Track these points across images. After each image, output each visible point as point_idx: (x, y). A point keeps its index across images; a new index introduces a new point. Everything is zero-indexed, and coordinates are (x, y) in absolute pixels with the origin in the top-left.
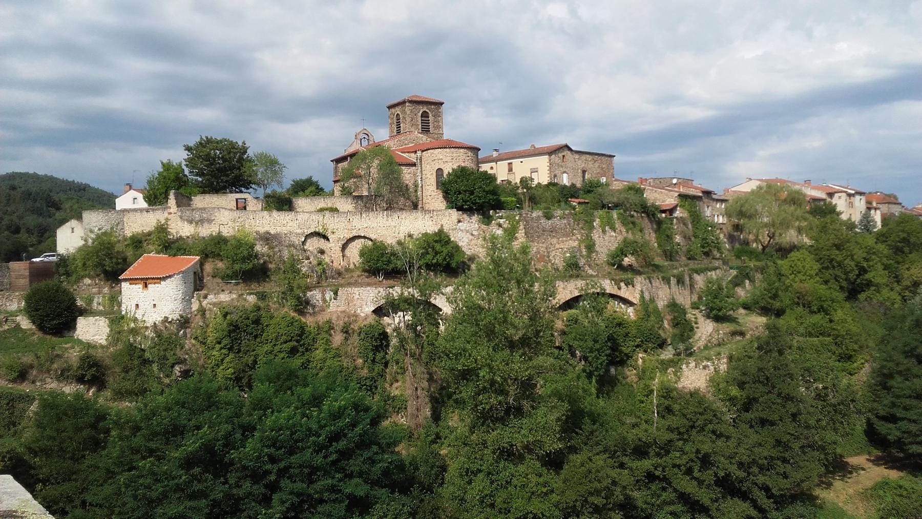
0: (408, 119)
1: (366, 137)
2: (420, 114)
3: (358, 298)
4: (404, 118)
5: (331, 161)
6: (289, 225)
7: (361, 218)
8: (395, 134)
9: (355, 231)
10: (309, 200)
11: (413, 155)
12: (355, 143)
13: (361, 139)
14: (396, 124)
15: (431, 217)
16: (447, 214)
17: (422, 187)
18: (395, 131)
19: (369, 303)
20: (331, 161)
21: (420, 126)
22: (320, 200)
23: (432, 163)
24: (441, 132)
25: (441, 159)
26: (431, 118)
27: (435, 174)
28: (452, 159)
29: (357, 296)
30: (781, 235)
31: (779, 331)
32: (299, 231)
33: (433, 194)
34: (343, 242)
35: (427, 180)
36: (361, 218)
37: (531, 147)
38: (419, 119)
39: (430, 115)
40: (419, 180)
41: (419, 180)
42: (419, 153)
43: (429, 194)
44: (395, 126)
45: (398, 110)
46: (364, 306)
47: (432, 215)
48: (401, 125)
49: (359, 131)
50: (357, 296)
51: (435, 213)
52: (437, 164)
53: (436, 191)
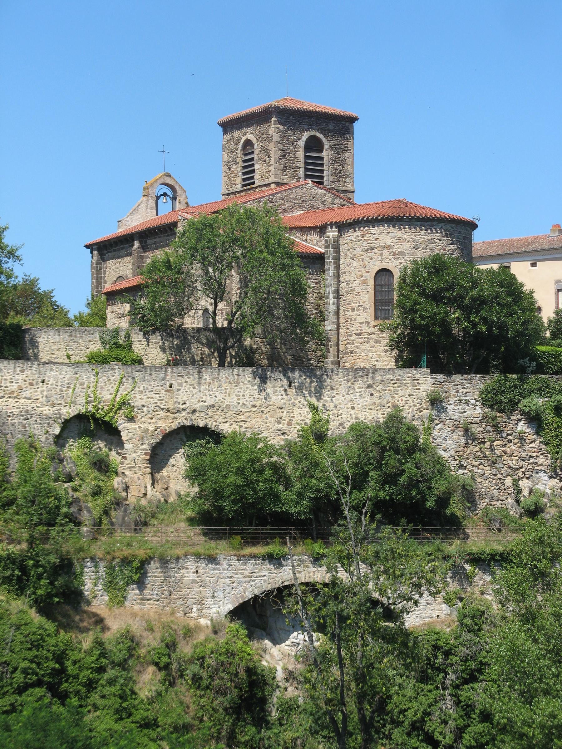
0: (275, 153)
1: (169, 192)
2: (302, 143)
3: (194, 581)
4: (264, 150)
5: (87, 247)
6: (24, 394)
7: (199, 384)
8: (239, 187)
9: (184, 413)
10: (66, 336)
11: (314, 237)
12: (143, 206)
13: (158, 198)
14: (241, 164)
15: (369, 386)
16: (408, 380)
17: (337, 313)
18: (239, 180)
19: (220, 594)
20: (87, 247)
21: (302, 171)
22: (91, 337)
23: (367, 257)
24: (349, 188)
25: (389, 247)
26: (326, 154)
27: (371, 282)
28: (416, 248)
29: (192, 576)
30: (429, 488)
31: (8, 665)
32: (47, 411)
33: (366, 329)
34: (153, 441)
35: (350, 297)
36: (199, 384)
37: (553, 230)
38: (301, 154)
39: (326, 147)
40: (331, 296)
41: (331, 296)
42: (332, 233)
43: (355, 328)
44: (238, 169)
45: (250, 134)
46: (210, 601)
47: (371, 382)
48: (256, 167)
49: (153, 180)
50: (192, 576)
51: (378, 377)
52: (377, 259)
53: (373, 323)
